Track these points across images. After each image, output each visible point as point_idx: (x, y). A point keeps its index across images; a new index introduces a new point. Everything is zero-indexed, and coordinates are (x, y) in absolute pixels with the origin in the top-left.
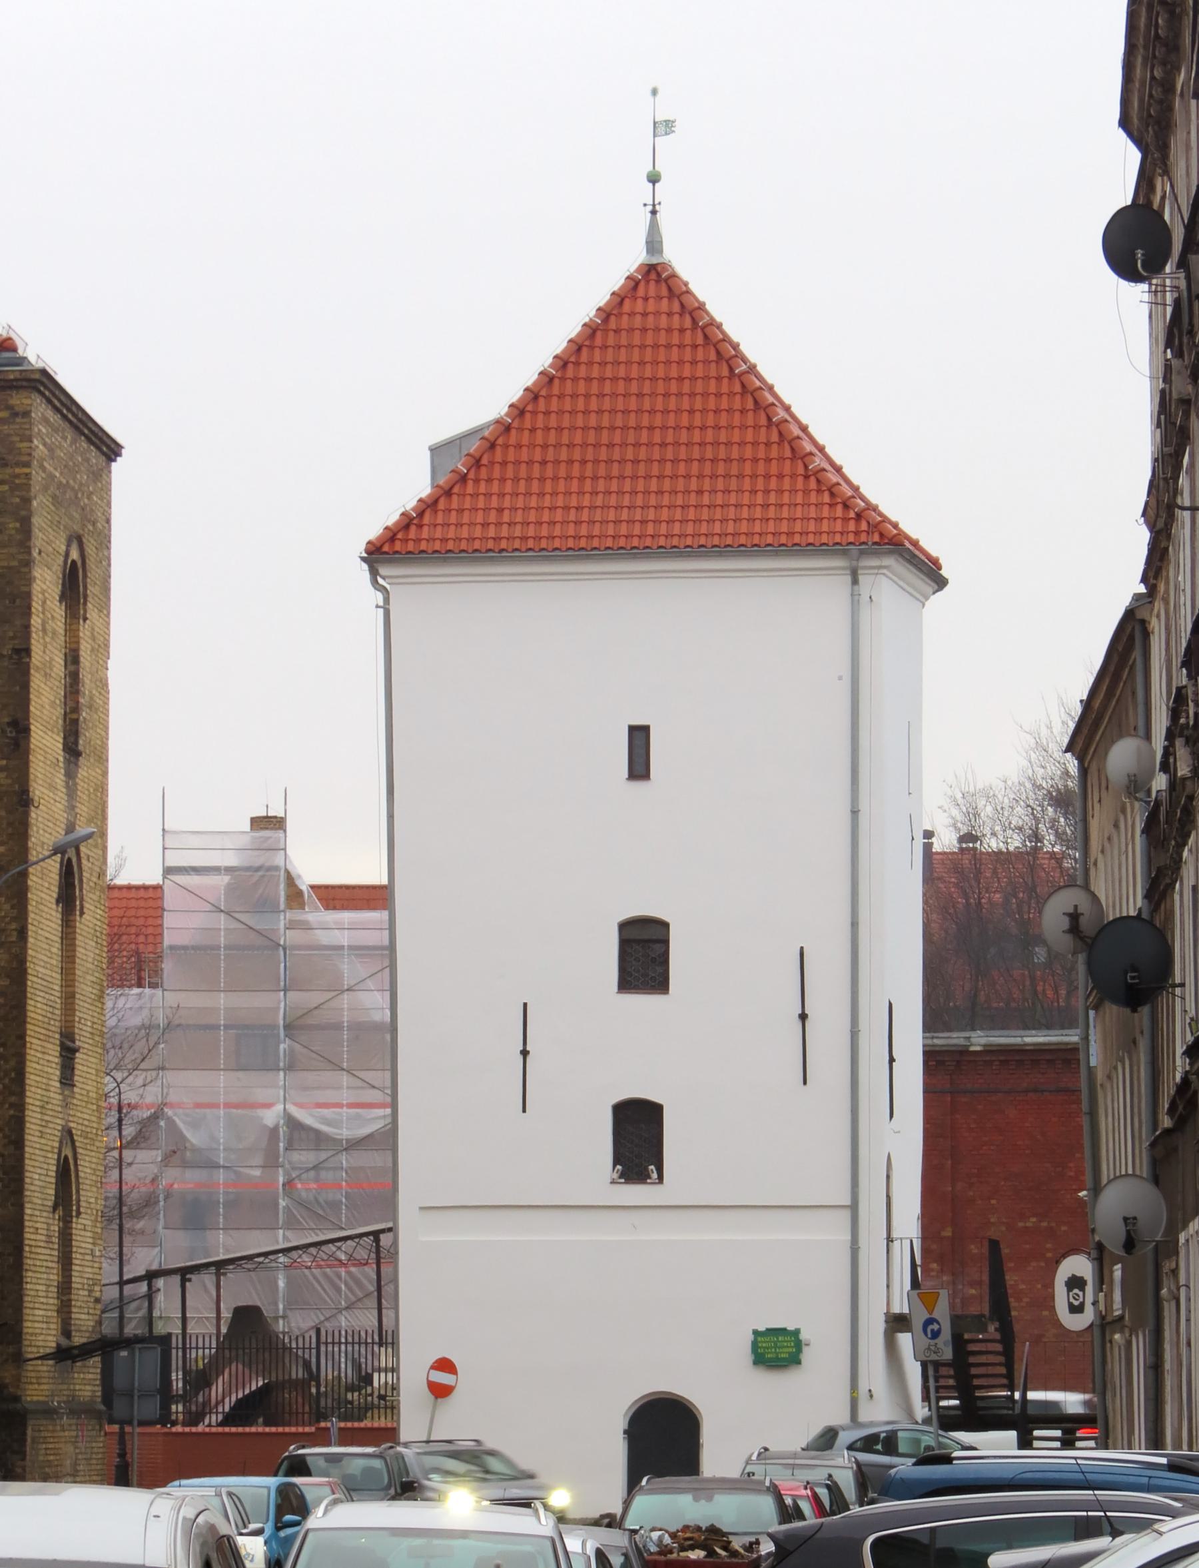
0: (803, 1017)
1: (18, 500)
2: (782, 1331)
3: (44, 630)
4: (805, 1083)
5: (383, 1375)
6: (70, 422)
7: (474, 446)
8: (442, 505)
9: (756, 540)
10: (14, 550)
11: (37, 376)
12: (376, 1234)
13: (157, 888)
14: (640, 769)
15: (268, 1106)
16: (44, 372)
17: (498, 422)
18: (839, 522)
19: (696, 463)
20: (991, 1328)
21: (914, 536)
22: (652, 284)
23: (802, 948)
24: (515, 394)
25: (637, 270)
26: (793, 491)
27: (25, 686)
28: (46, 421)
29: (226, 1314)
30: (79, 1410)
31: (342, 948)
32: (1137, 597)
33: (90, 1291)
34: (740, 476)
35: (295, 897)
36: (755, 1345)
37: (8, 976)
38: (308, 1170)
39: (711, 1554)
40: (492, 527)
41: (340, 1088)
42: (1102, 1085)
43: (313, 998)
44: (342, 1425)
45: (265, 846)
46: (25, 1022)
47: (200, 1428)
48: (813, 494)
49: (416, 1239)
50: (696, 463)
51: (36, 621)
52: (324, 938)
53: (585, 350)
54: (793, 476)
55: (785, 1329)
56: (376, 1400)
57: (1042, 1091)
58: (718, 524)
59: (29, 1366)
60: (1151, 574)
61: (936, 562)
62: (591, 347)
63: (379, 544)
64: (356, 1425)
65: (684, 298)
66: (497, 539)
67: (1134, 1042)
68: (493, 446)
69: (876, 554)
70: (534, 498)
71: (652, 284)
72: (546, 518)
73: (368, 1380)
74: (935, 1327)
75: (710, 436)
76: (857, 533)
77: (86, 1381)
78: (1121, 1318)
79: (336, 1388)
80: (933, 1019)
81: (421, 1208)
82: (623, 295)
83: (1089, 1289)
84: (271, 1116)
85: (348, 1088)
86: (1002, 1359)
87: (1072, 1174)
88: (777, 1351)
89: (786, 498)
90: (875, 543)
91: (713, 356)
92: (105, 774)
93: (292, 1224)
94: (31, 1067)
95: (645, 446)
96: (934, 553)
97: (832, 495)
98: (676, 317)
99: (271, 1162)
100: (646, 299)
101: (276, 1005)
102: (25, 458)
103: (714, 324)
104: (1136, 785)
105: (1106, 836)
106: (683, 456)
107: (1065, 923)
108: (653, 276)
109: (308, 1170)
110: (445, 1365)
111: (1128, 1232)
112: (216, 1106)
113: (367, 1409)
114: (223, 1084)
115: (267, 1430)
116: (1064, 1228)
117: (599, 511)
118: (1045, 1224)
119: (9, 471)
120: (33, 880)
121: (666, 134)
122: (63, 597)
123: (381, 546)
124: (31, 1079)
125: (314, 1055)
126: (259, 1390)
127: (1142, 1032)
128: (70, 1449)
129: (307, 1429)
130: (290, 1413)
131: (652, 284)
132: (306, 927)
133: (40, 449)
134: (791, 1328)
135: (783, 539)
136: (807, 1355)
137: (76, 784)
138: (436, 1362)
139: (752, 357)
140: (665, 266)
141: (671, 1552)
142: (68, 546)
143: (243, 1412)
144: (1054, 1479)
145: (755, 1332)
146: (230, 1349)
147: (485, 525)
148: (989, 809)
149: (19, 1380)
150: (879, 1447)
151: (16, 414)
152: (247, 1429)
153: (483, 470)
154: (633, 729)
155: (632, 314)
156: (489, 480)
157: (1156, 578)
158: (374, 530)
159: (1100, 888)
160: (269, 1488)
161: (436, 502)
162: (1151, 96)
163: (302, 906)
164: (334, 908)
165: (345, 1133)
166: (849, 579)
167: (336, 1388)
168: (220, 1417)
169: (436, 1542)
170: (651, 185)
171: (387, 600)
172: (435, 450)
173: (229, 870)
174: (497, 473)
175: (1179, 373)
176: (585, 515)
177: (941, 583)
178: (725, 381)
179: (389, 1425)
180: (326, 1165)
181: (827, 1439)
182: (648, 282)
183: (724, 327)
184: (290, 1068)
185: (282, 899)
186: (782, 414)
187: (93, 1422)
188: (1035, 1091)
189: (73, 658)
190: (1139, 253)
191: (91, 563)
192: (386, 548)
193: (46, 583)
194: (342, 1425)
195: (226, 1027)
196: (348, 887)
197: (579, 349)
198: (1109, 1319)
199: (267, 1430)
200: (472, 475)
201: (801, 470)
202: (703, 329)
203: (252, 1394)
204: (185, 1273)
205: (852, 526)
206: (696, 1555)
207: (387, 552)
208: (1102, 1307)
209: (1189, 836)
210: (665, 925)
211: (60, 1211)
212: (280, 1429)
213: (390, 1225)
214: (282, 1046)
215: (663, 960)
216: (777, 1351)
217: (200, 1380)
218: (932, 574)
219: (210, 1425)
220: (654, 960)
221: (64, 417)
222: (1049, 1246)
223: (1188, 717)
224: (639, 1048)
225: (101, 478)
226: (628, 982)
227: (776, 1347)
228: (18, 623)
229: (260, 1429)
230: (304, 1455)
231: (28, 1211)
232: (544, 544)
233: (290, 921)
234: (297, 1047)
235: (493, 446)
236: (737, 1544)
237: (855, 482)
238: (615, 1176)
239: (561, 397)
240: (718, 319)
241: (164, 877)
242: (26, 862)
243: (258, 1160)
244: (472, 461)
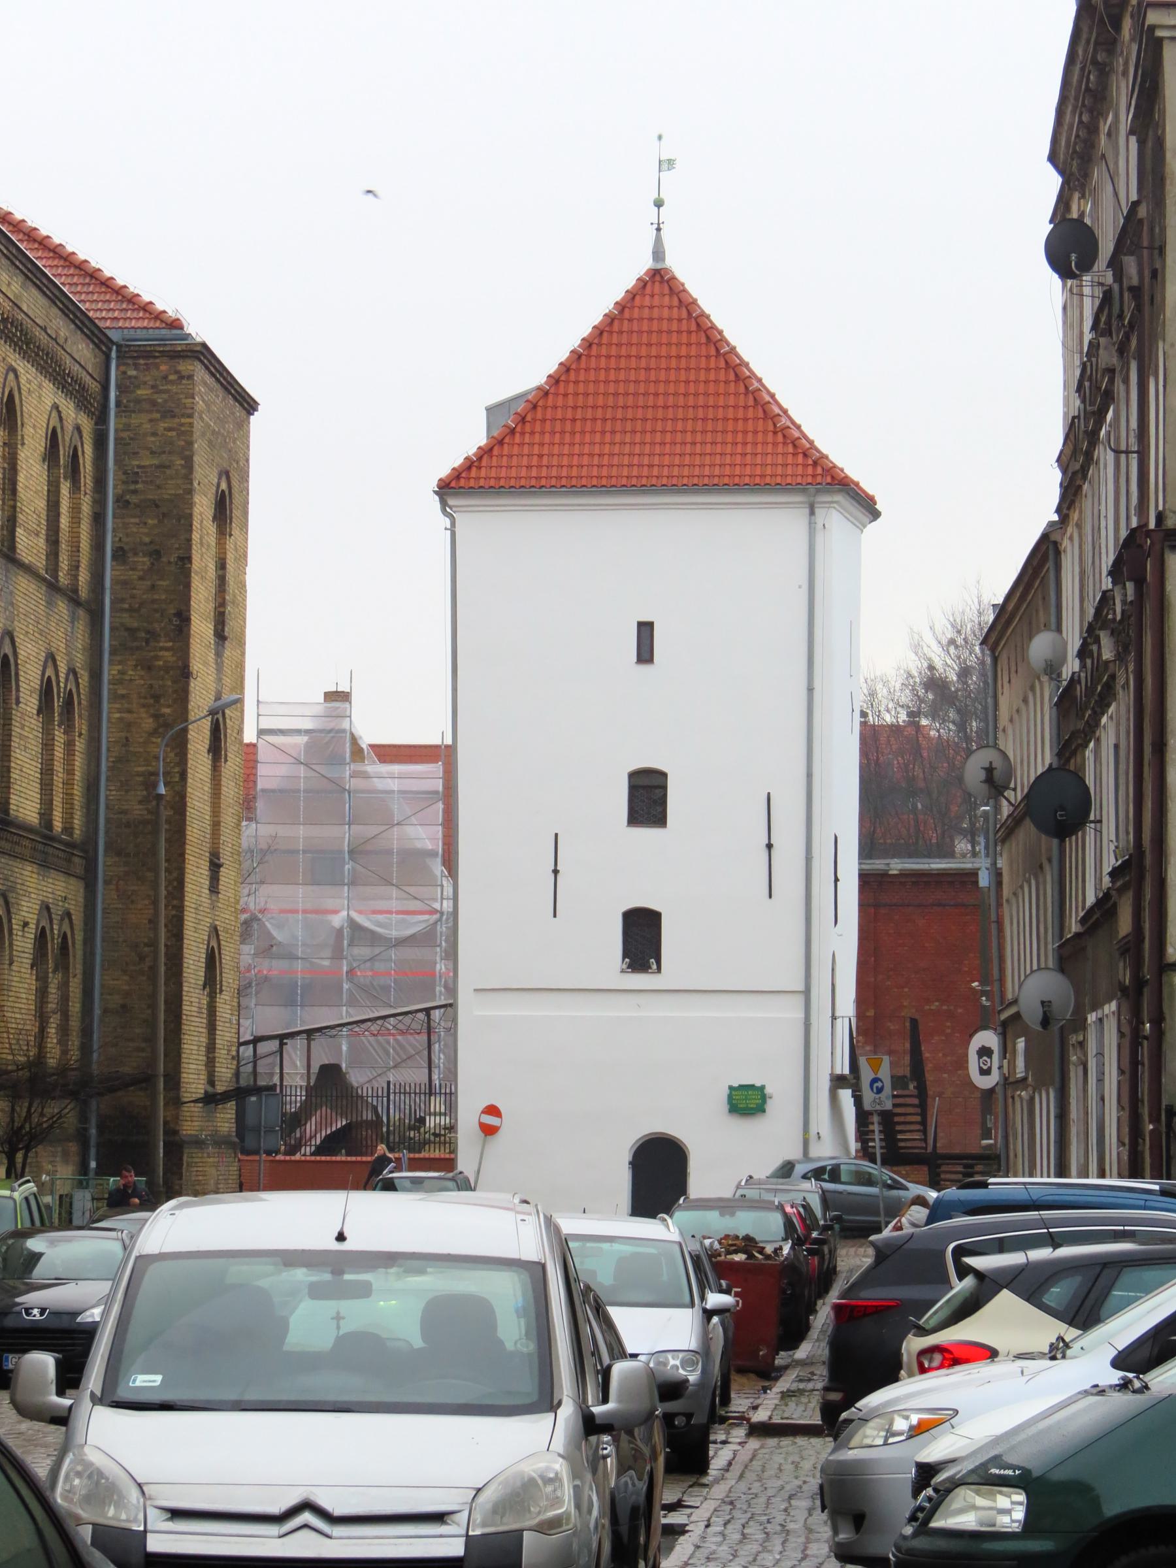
0: (769, 846)
1: (183, 443)
3: (201, 544)
4: (770, 897)
6: (222, 384)
7: (520, 407)
8: (496, 451)
9: (737, 480)
10: (179, 482)
11: (198, 348)
12: (427, 1011)
13: (254, 745)
14: (646, 656)
15: (336, 912)
16: (204, 345)
17: (539, 388)
18: (800, 467)
19: (690, 422)
20: (911, 1086)
21: (856, 479)
24: (552, 367)
25: (646, 274)
26: (765, 443)
27: (188, 586)
28: (205, 384)
29: (315, 1069)
30: (220, 1142)
32: (1051, 524)
33: (229, 1051)
34: (735, 432)
35: (357, 753)
36: (730, 1097)
37: (172, 808)
38: (365, 961)
39: (751, 1256)
40: (534, 469)
41: (390, 898)
42: (1008, 901)
44: (412, 1155)
45: (334, 714)
46: (185, 843)
47: (297, 1157)
48: (781, 445)
49: (472, 1012)
50: (690, 422)
51: (195, 536)
52: (379, 784)
53: (605, 334)
54: (765, 432)
55: (753, 1086)
57: (944, 906)
58: (707, 468)
59: (185, 1108)
60: (1065, 506)
61: (872, 500)
62: (611, 332)
64: (417, 1156)
65: (682, 295)
66: (538, 478)
67: (1041, 867)
68: (535, 407)
69: (828, 492)
70: (567, 446)
71: (657, 284)
72: (575, 462)
73: (422, 1121)
74: (879, 1084)
75: (701, 400)
76: (814, 476)
77: (225, 1119)
78: (1025, 1079)
80: (869, 847)
83: (995, 1057)
84: (338, 920)
86: (918, 1110)
88: (747, 1102)
89: (759, 449)
91: (703, 340)
92: (243, 654)
93: (352, 1002)
94: (189, 877)
95: (649, 407)
96: (870, 492)
97: (795, 446)
98: (676, 310)
99: (338, 955)
100: (652, 296)
101: (343, 835)
102: (190, 411)
103: (703, 315)
104: (1052, 669)
105: (1015, 708)
106: (680, 416)
107: (982, 775)
108: (658, 278)
109: (365, 961)
110: (492, 1110)
111: (1045, 1013)
112: (295, 911)
113: (425, 1144)
114: (300, 895)
115: (349, 1159)
116: (960, 1011)
117: (616, 457)
118: (945, 1007)
119: (177, 420)
120: (192, 735)
122: (215, 518)
124: (189, 887)
126: (343, 1127)
127: (1050, 860)
128: (213, 1171)
130: (367, 1146)
131: (657, 284)
132: (366, 776)
133: (200, 405)
134: (758, 1084)
135: (757, 480)
136: (770, 1106)
137: (222, 662)
139: (733, 342)
140: (667, 270)
141: (720, 1255)
142: (220, 479)
143: (330, 1145)
144: (1072, 1198)
145: (731, 1088)
146: (316, 1097)
147: (529, 467)
148: (885, 691)
149: (177, 1118)
150: (826, 1177)
151: (182, 378)
152: (334, 1158)
153: (528, 424)
154: (641, 625)
155: (641, 307)
156: (532, 433)
157: (1069, 508)
158: (444, 471)
159: (1009, 745)
161: (491, 449)
162: (1077, 136)
163: (362, 759)
164: (384, 762)
165: (394, 933)
166: (807, 511)
168: (313, 1148)
169: (589, 1245)
171: (453, 524)
172: (489, 410)
173: (307, 732)
174: (538, 428)
175: (1106, 348)
176: (605, 461)
177: (875, 515)
178: (713, 359)
179: (447, 1156)
181: (786, 1170)
182: (654, 282)
183: (712, 318)
184: (353, 883)
185: (348, 755)
186: (756, 384)
187: (230, 1151)
188: (940, 905)
189: (222, 565)
190: (1073, 257)
191: (235, 491)
192: (453, 484)
193: (203, 507)
194: (412, 1155)
195: (304, 852)
196: (395, 746)
197: (601, 333)
198: (1011, 1080)
199: (349, 1159)
200: (518, 429)
201: (771, 428)
202: (696, 319)
203: (338, 1131)
204: (282, 1038)
205: (810, 470)
206: (740, 1257)
207: (455, 487)
208: (1005, 1070)
209: (1109, 706)
210: (664, 775)
211: (208, 989)
212: (359, 1159)
213: (451, 1001)
215: (663, 801)
216: (747, 1102)
217: (296, 1121)
218: (868, 507)
219: (305, 1155)
220: (655, 802)
221: (217, 380)
223: (1115, 613)
224: (646, 868)
225: (242, 427)
228: (182, 537)
229: (344, 1158)
230: (392, 1178)
231: (185, 989)
232: (574, 482)
234: (358, 867)
235: (535, 407)
236: (769, 1249)
237: (811, 437)
238: (625, 966)
239: (587, 370)
240: (707, 312)
241: (258, 737)
242: (186, 721)
243: (327, 953)
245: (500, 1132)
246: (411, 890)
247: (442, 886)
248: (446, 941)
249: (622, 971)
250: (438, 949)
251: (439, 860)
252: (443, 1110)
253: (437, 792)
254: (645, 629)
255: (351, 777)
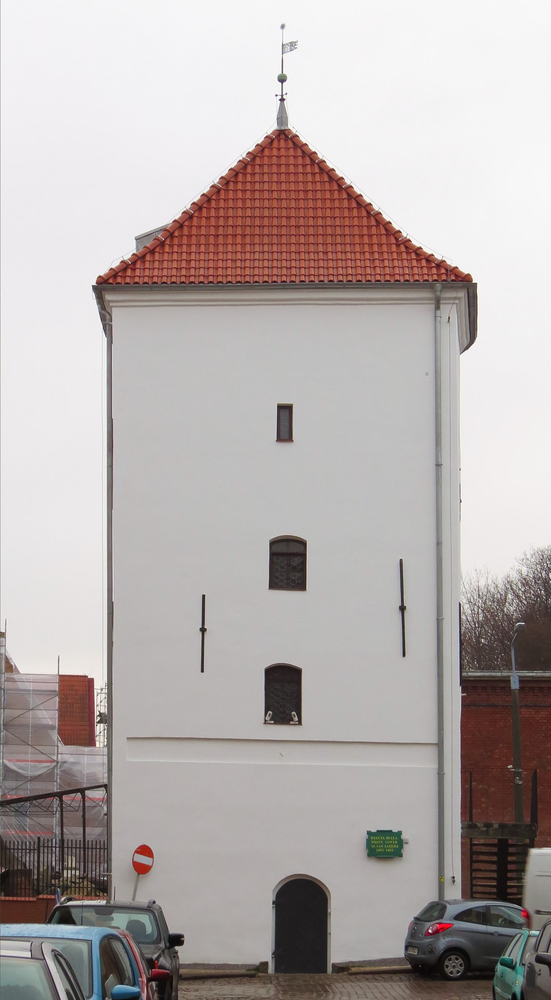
0: (402, 609)
2: (389, 833)
4: (404, 655)
5: (69, 872)
8: (148, 257)
22: (282, 142)
23: (401, 560)
25: (273, 133)
31: (30, 690)
36: (369, 842)
43: (17, 713)
55: (391, 831)
56: (69, 884)
63: (106, 278)
79: (45, 876)
81: (128, 738)
82: (264, 146)
85: (31, 753)
87: (497, 756)
88: (384, 847)
90: (453, 280)
108: (283, 136)
110: (145, 850)
115: (7, 898)
116: (493, 789)
118: (481, 786)
121: (291, 50)
123: (108, 279)
125: (16, 738)
129: (31, 899)
130: (21, 889)
134: (395, 830)
138: (139, 848)
145: (369, 833)
158: (103, 271)
160: (90, 943)
165: (30, 773)
166: (433, 306)
167: (45, 876)
170: (280, 83)
180: (21, 787)
182: (279, 140)
185: (3, 668)
192: (111, 281)
199: (7, 898)
200: (168, 242)
212: (15, 899)
214: (2, 734)
216: (384, 847)
220: (294, 568)
222: (483, 800)
224: (285, 627)
226: (276, 583)
227: (384, 844)
230: (68, 907)
233: (7, 678)
234: (9, 734)
238: (268, 718)
244: (168, 234)
245: (153, 870)
246: (40, 748)
247: (58, 746)
248: (60, 779)
249: (266, 722)
250: (55, 783)
251: (56, 731)
252: (74, 866)
253: (55, 691)
254: (285, 413)
255: (5, 681)
